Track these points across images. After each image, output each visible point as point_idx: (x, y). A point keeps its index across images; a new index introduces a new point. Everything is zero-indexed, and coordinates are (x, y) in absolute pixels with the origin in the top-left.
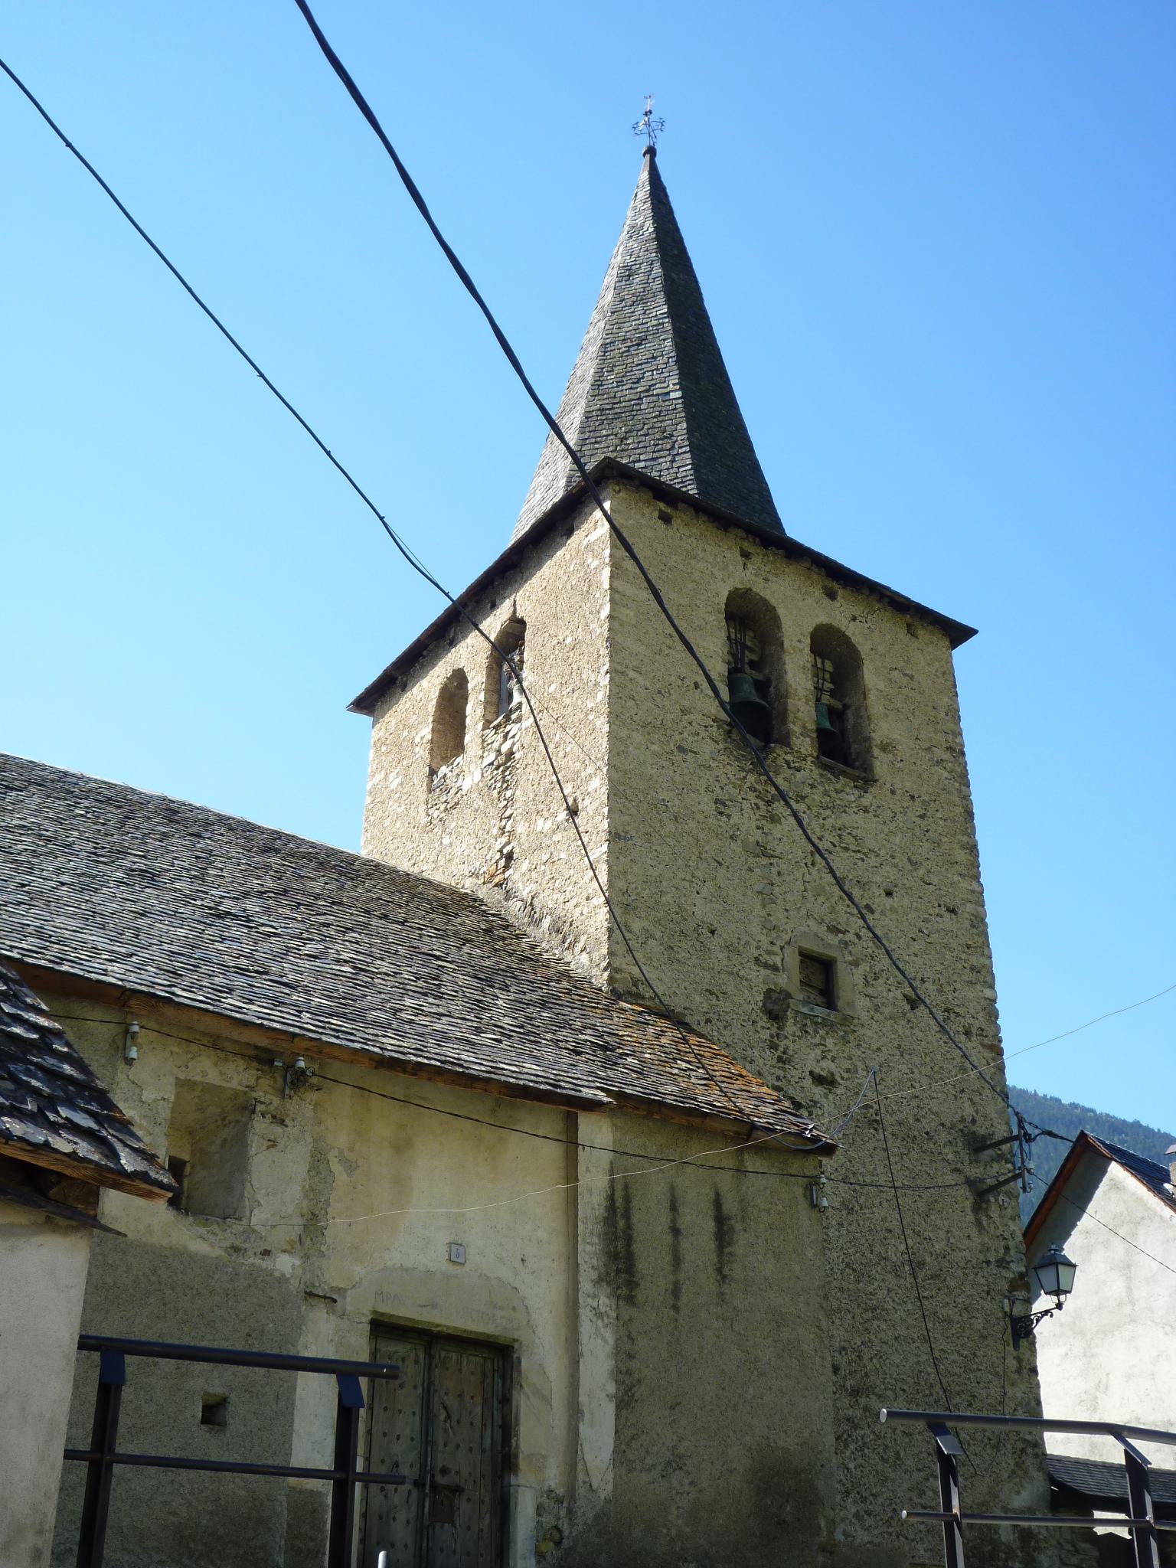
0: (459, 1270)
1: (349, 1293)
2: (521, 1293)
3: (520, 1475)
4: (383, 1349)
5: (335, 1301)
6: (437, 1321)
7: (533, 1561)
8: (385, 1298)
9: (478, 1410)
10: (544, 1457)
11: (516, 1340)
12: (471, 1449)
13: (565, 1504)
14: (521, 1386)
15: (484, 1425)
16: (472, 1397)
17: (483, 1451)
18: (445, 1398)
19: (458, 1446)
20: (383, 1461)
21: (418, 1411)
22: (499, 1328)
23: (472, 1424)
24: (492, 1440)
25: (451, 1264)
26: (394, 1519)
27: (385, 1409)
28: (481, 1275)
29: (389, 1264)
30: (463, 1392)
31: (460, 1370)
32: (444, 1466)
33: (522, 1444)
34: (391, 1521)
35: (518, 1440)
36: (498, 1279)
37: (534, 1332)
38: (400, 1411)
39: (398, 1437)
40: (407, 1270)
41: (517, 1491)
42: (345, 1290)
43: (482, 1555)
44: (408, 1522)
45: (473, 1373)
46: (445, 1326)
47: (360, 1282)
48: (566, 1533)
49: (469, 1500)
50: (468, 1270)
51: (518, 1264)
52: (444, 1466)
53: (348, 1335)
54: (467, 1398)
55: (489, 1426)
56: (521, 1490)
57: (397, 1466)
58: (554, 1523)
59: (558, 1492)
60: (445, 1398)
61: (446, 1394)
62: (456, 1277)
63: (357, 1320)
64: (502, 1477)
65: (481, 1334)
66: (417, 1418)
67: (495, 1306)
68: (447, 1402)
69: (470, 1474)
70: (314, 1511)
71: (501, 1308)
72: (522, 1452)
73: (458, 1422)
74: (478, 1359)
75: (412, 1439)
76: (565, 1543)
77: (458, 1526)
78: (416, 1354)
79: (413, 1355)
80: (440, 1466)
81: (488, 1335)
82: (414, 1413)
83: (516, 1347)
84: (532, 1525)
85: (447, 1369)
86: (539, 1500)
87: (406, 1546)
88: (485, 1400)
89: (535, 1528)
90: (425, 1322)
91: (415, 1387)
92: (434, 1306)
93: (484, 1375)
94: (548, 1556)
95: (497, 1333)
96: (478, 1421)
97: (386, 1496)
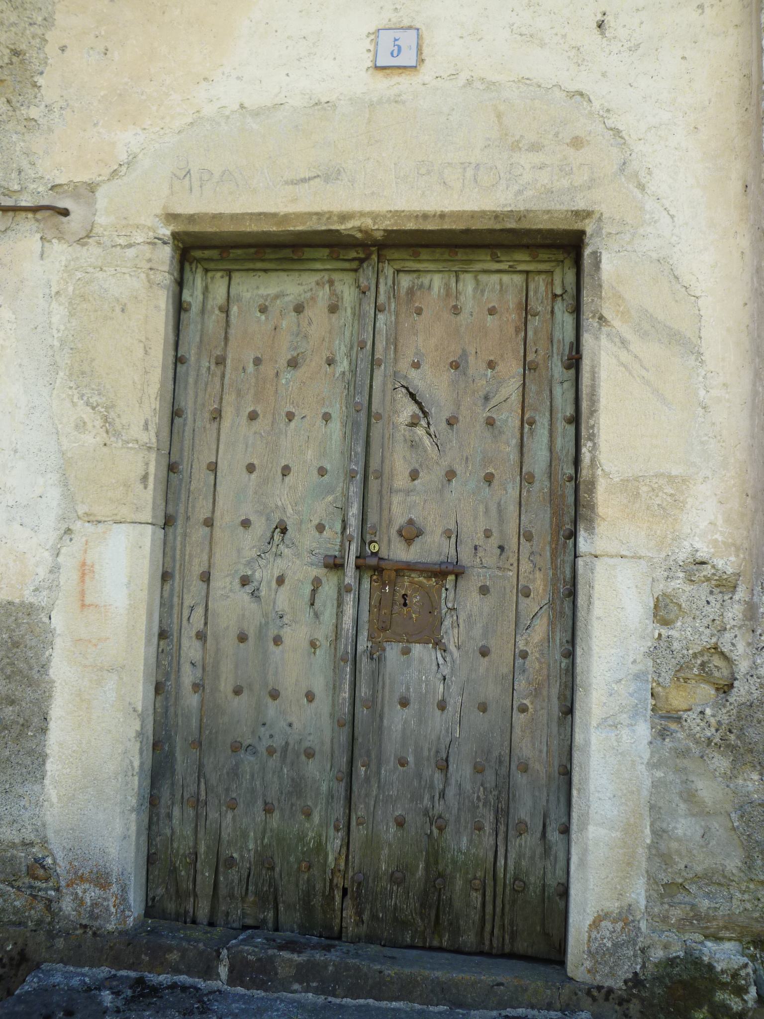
0: (403, 83)
1: (100, 193)
2: (596, 104)
3: (601, 528)
4: (248, 295)
5: (65, 213)
6: (337, 207)
7: (644, 730)
8: (196, 184)
9: (511, 389)
10: (680, 482)
11: (588, 214)
12: (489, 479)
13: (741, 594)
14: (601, 318)
15: (526, 423)
16: (491, 365)
17: (527, 479)
18: (413, 374)
19: (451, 475)
20: (246, 524)
21: (337, 410)
22: (529, 193)
23: (490, 423)
24: (551, 450)
25: (380, 74)
26: (277, 641)
27: (253, 416)
28: (469, 83)
29: (209, 110)
30: (464, 354)
31: (456, 310)
32: (411, 522)
33: (603, 457)
34: (271, 644)
35: (595, 447)
36: (524, 81)
37: (642, 187)
38: (290, 416)
39: (286, 471)
40: (256, 114)
41: (592, 570)
42: (92, 188)
43: (523, 709)
44: (313, 644)
45: (492, 311)
46: (362, 214)
47: (131, 162)
48: (743, 666)
49: (484, 590)
50: (427, 79)
51: (591, 39)
52: (411, 522)
53: (100, 275)
54: (476, 366)
55: (543, 421)
56: (601, 568)
57: (284, 531)
58: (706, 639)
59: (720, 563)
60: (413, 374)
61: (416, 365)
62: (397, 100)
63: (122, 241)
64: (573, 535)
65: (473, 215)
66: (336, 427)
67: (515, 147)
68: (416, 382)
69: (488, 534)
70: (16, 645)
71: (535, 147)
72: (607, 475)
73: (450, 423)
74: (506, 278)
75: (322, 472)
76: (742, 691)
77: (452, 648)
78: (333, 293)
79: (324, 294)
80: (400, 520)
81: (496, 216)
82: (327, 417)
83: (589, 231)
84: (639, 647)
85: (419, 312)
86: (661, 587)
87: (310, 697)
88: (528, 367)
89: (649, 654)
90: (310, 214)
91: (330, 362)
92: (331, 175)
93: (526, 310)
94: (692, 719)
95: (521, 207)
96: (510, 419)
97: (255, 594)
